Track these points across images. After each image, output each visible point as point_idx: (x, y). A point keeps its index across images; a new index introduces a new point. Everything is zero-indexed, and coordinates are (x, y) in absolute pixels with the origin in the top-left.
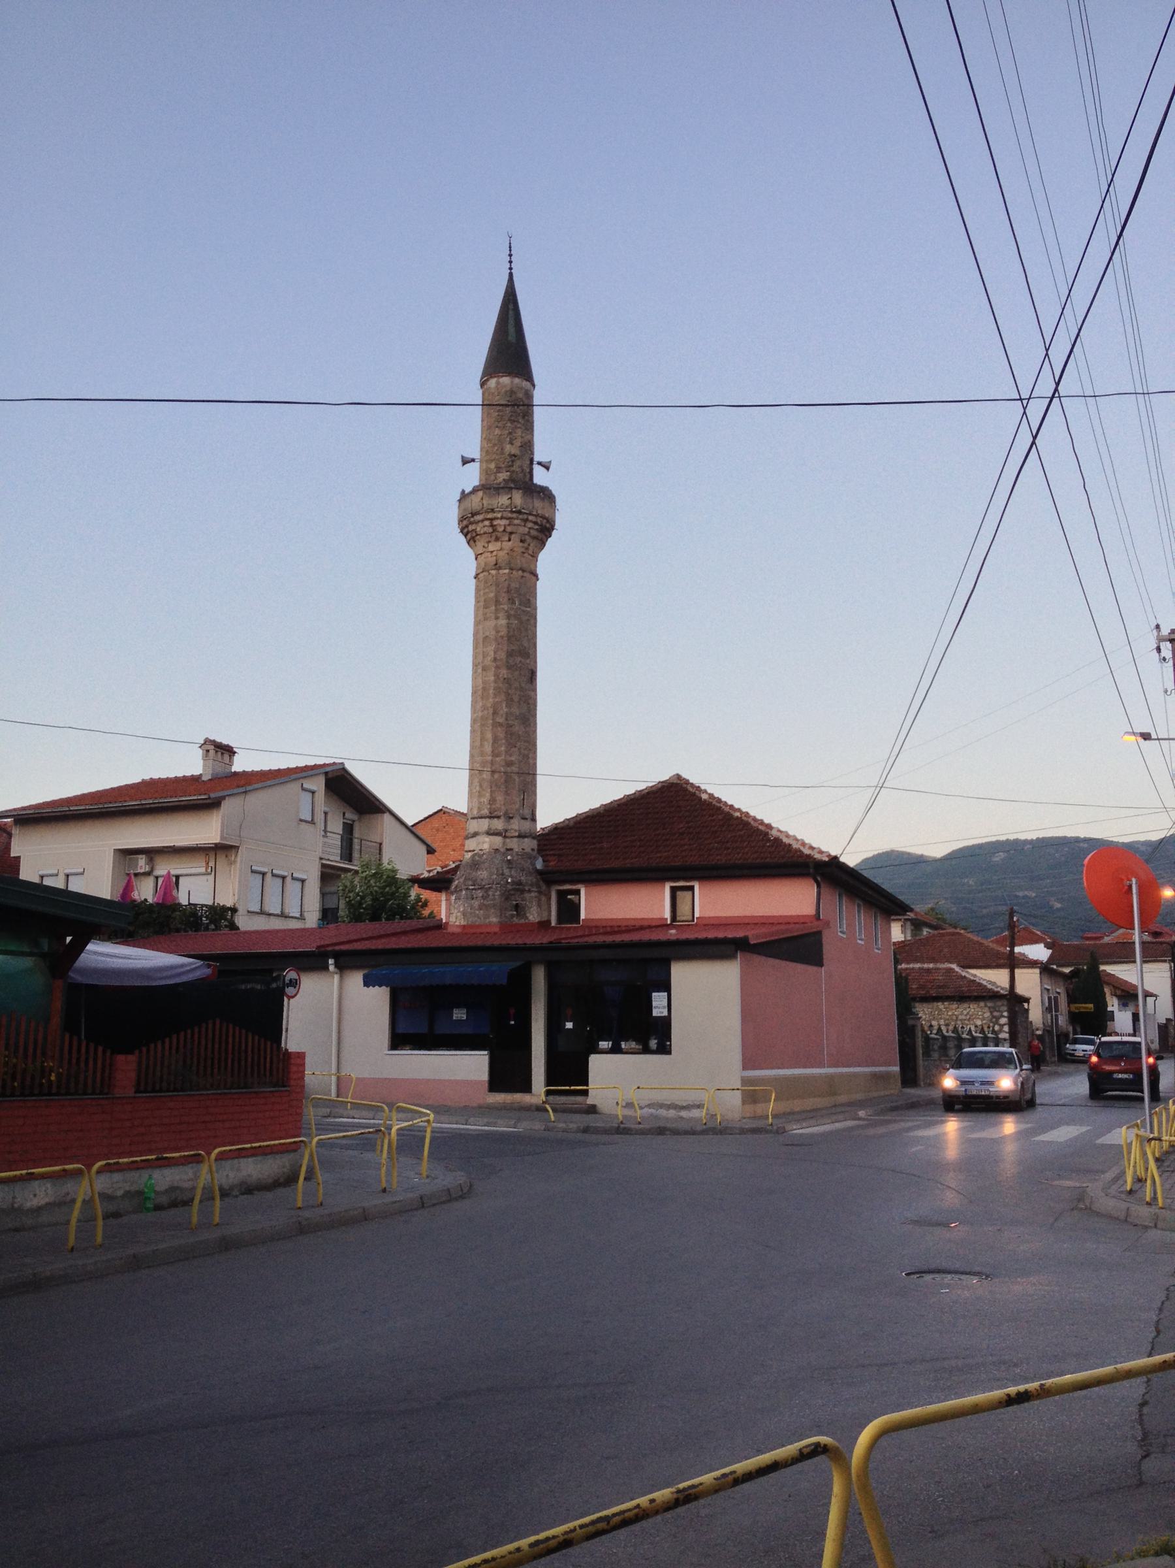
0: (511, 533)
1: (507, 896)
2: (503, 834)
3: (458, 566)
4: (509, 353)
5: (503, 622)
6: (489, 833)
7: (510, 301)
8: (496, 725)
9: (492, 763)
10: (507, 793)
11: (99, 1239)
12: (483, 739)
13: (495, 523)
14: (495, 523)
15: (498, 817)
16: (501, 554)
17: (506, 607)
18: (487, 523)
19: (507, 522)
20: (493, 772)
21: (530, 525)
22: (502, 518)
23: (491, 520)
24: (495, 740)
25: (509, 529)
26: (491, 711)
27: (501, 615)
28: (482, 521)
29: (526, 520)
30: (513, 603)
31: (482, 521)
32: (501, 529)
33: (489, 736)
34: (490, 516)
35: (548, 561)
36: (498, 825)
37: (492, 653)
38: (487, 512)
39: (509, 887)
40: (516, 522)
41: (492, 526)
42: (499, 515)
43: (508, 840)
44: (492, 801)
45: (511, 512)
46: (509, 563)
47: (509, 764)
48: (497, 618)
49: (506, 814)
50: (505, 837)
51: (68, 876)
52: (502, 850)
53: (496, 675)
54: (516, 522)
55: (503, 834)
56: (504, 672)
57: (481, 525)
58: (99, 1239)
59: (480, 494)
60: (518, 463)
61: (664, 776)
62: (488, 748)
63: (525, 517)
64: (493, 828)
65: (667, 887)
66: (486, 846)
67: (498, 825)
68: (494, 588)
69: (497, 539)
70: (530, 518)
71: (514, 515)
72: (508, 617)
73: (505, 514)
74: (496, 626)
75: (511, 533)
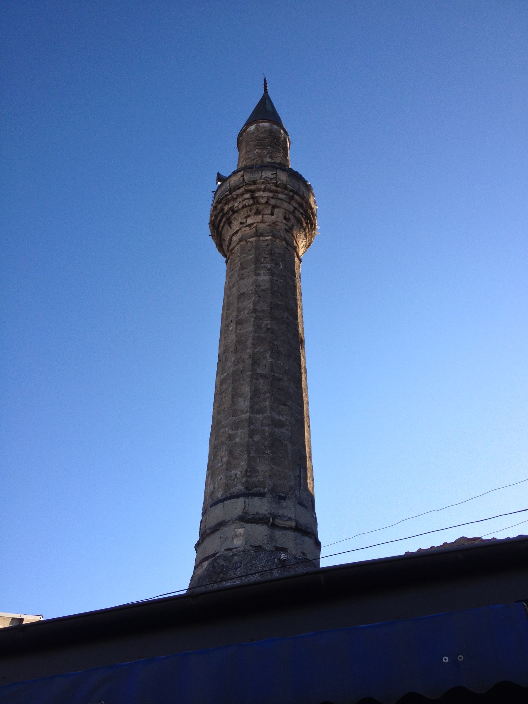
0: (274, 207)
2: (269, 521)
3: (204, 285)
5: (264, 278)
6: (245, 519)
7: (265, 80)
8: (255, 376)
9: (250, 421)
12: (235, 395)
13: (257, 195)
14: (257, 195)
15: (261, 495)
16: (262, 225)
18: (247, 196)
19: (271, 195)
20: (251, 434)
21: (295, 204)
23: (252, 192)
24: (255, 393)
25: (272, 202)
26: (249, 362)
28: (242, 194)
29: (292, 198)
30: (277, 264)
31: (242, 194)
32: (263, 201)
33: (246, 389)
34: (252, 187)
35: (314, 263)
36: (261, 506)
37: (251, 305)
38: (249, 184)
41: (253, 198)
42: (263, 187)
43: (278, 533)
44: (251, 471)
45: (277, 186)
46: (271, 232)
48: (257, 275)
49: (272, 491)
50: (274, 526)
52: (268, 547)
53: (257, 327)
55: (269, 521)
56: (267, 322)
57: (239, 200)
59: (241, 173)
62: (244, 404)
63: (291, 194)
64: (252, 511)
66: (238, 542)
67: (261, 506)
68: (253, 251)
69: (258, 213)
70: (296, 197)
73: (269, 186)
74: (255, 281)
75: (274, 207)
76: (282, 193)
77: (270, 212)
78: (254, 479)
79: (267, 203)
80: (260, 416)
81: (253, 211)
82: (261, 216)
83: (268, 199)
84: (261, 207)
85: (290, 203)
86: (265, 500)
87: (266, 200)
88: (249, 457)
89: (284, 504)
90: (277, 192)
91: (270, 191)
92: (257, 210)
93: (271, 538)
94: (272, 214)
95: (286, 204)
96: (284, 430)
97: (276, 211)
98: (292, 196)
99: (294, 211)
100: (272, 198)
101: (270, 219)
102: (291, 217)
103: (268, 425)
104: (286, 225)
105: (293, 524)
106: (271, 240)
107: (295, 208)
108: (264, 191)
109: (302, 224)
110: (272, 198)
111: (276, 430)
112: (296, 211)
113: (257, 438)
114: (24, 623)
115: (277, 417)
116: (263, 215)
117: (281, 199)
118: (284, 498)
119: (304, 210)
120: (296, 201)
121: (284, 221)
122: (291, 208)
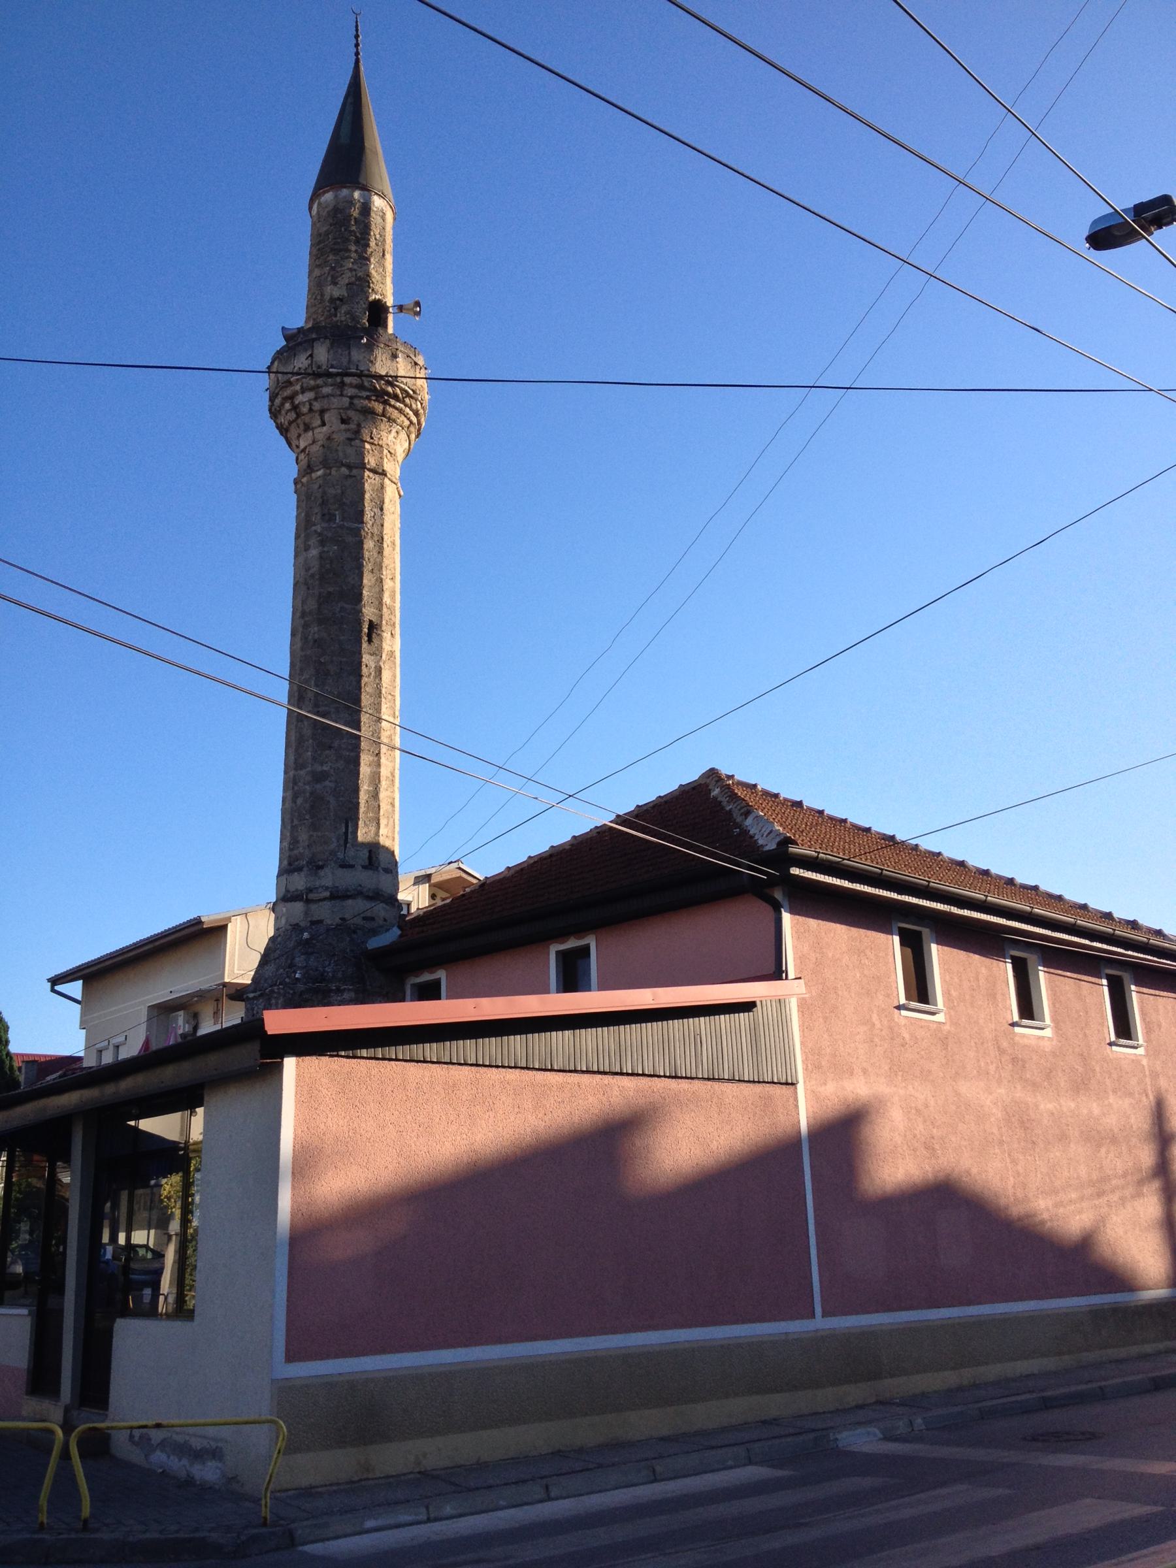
1: (1023, 1061)
4: (345, 161)
10: (314, 827)
11: (86, 1511)
17: (318, 528)
21: (350, 391)
22: (303, 391)
23: (291, 398)
25: (317, 406)
27: (313, 541)
34: (288, 392)
39: (301, 987)
40: (326, 390)
43: (313, 907)
47: (319, 777)
50: (308, 901)
51: (100, 1051)
54: (326, 390)
58: (86, 1511)
60: (344, 309)
61: (691, 774)
63: (338, 379)
64: (292, 889)
65: (554, 949)
69: (307, 428)
70: (347, 380)
71: (320, 381)
72: (322, 543)
75: (322, 412)
76: (326, 385)
77: (319, 422)
78: (295, 852)
79: (311, 410)
80: (302, 773)
81: (302, 427)
82: (310, 433)
83: (311, 405)
84: (307, 419)
85: (342, 395)
86: (303, 874)
87: (307, 406)
88: (293, 827)
89: (322, 873)
90: (318, 387)
91: (311, 389)
92: (305, 424)
93: (306, 913)
94: (323, 424)
95: (335, 400)
96: (327, 783)
97: (327, 416)
98: (343, 383)
99: (351, 403)
100: (316, 399)
101: (321, 433)
102: (351, 413)
103: (309, 783)
104: (347, 430)
105: (327, 894)
106: (325, 475)
107: (351, 398)
108: (303, 392)
109: (372, 412)
110: (316, 399)
111: (318, 786)
112: (356, 401)
113: (299, 801)
114: (413, 909)
115: (319, 768)
116: (313, 429)
117: (328, 396)
118: (321, 867)
119: (369, 390)
120: (351, 386)
121: (343, 426)
122: (346, 400)
